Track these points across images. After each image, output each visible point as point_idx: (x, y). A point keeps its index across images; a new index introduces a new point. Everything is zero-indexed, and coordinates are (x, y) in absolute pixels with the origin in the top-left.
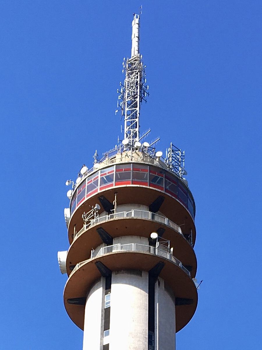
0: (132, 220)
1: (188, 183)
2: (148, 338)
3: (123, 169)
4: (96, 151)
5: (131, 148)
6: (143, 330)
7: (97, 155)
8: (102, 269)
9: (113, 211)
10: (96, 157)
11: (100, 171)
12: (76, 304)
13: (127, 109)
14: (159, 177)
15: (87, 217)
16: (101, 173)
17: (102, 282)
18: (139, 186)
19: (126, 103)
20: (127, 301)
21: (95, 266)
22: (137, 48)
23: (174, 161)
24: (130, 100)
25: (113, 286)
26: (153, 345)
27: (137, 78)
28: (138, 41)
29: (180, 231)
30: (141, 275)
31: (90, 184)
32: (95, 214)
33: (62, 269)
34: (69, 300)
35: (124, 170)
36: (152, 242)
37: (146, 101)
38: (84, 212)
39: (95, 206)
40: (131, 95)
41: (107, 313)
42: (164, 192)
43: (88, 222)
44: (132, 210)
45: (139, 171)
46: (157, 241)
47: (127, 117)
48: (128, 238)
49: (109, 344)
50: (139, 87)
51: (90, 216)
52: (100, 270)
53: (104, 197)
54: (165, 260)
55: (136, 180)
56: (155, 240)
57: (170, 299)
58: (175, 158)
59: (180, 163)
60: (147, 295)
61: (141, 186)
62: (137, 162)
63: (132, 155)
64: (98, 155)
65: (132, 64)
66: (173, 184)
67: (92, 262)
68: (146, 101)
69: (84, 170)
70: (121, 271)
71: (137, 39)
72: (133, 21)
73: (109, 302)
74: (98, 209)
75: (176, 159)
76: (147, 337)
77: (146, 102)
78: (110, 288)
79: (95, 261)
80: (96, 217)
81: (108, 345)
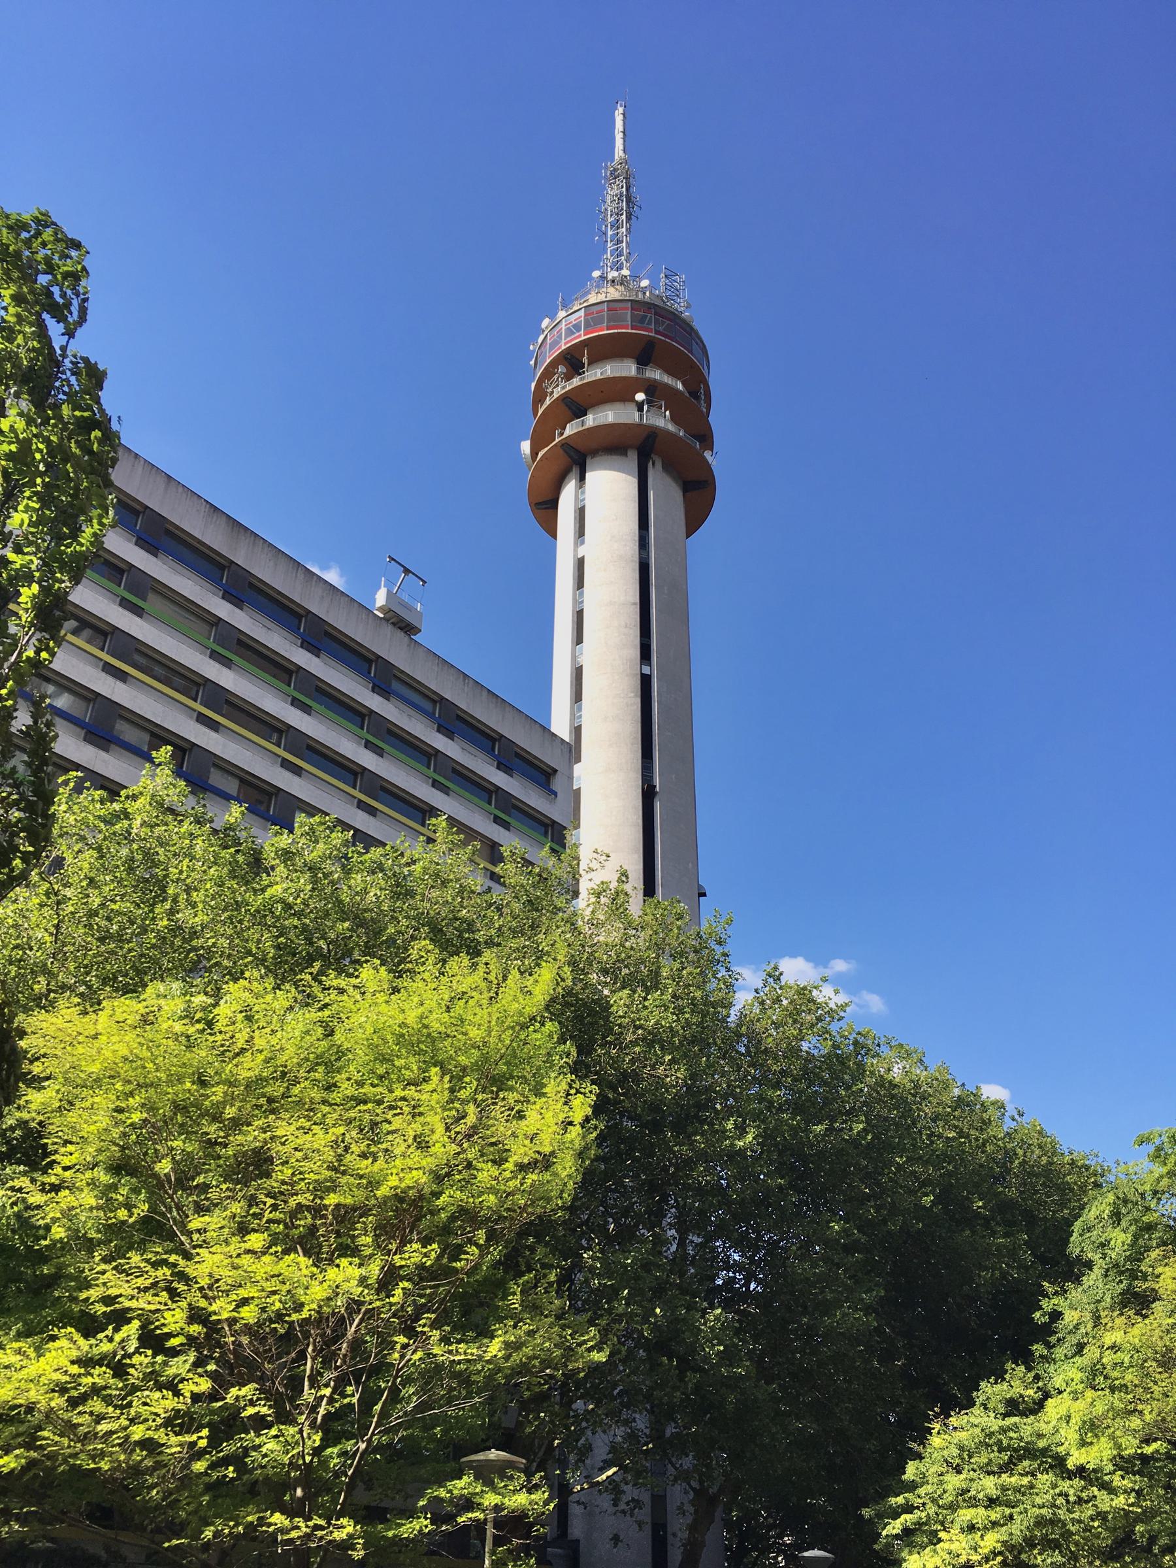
0: (608, 379)
12: (546, 507)
13: (610, 233)
17: (575, 472)
20: (606, 495)
21: (561, 452)
22: (621, 147)
25: (588, 475)
29: (680, 386)
30: (626, 455)
41: (581, 513)
48: (601, 407)
52: (570, 457)
56: (643, 402)
57: (674, 484)
69: (545, 322)
71: (621, 135)
76: (637, 538)
81: (583, 558)
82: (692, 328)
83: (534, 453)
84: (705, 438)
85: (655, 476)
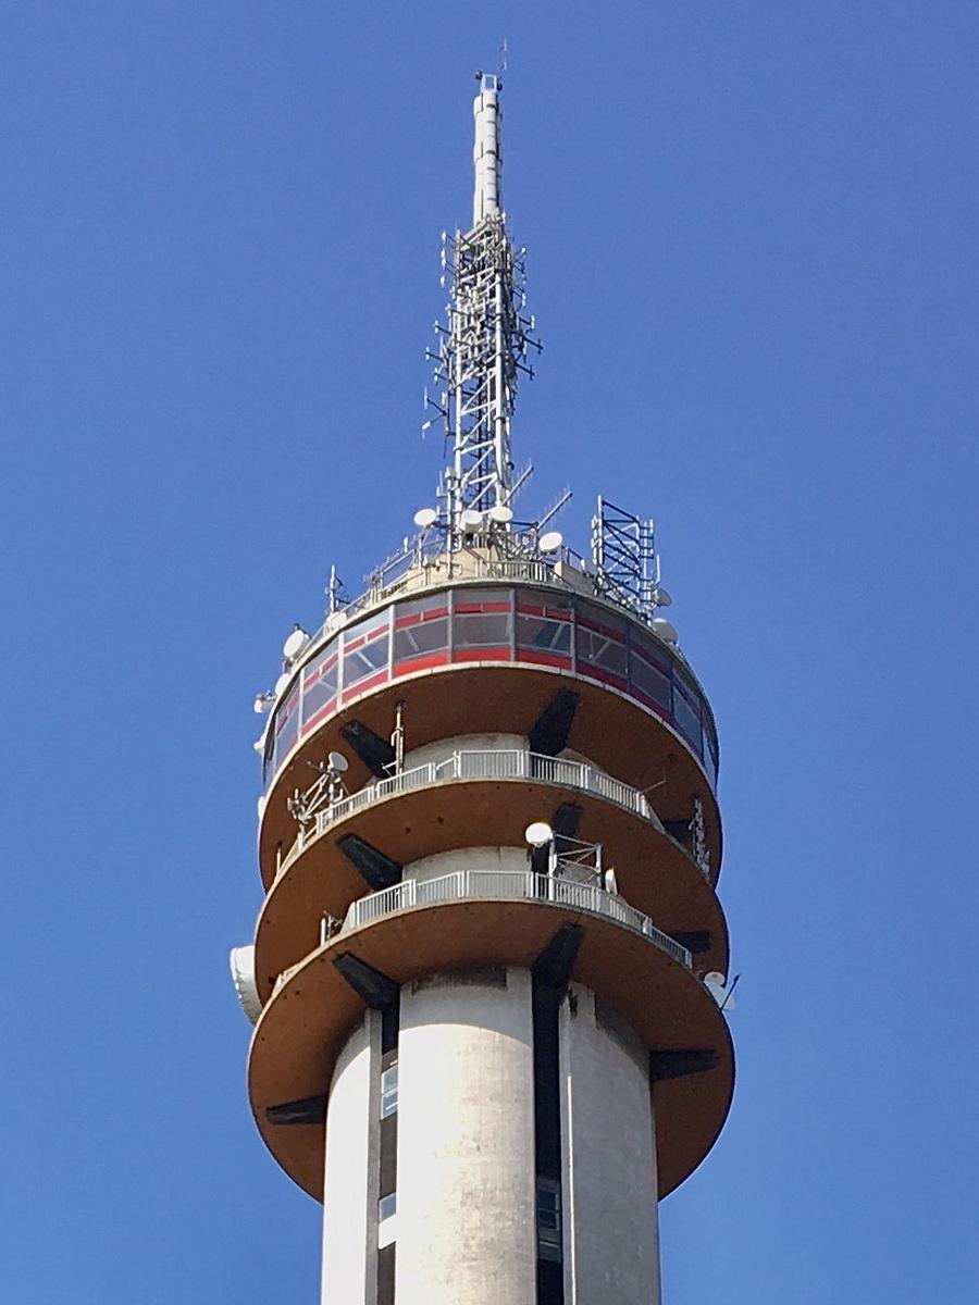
1: (675, 634)
2: (533, 1206)
3: (419, 615)
4: (333, 568)
5: (449, 536)
6: (516, 1176)
7: (338, 583)
8: (364, 981)
9: (394, 767)
10: (334, 591)
11: (341, 636)
12: (295, 1120)
13: (461, 412)
14: (604, 642)
15: (306, 807)
16: (346, 641)
17: (371, 1028)
18: (476, 664)
19: (459, 390)
20: (451, 1081)
22: (490, 192)
23: (616, 560)
24: (469, 377)
25: (405, 1036)
26: (558, 1228)
27: (493, 294)
28: (496, 165)
29: (642, 807)
31: (311, 687)
32: (331, 788)
33: (249, 1007)
34: (271, 1113)
35: (422, 618)
36: (538, 858)
37: (530, 372)
38: (297, 791)
39: (328, 763)
40: (473, 358)
42: (571, 673)
43: (312, 822)
44: (455, 753)
45: (479, 612)
46: (552, 850)
47: (462, 439)
48: (437, 861)
49: (394, 1244)
50: (498, 326)
51: (316, 801)
52: (355, 985)
53: (360, 725)
54: (582, 914)
55: (466, 645)
58: (620, 551)
59: (637, 563)
60: (529, 1049)
61: (485, 664)
62: (469, 581)
63: (452, 558)
64: (341, 584)
65: (474, 250)
66: (616, 643)
67: (322, 960)
68: (530, 372)
69: (295, 642)
70: (431, 980)
71: (489, 160)
72: (478, 100)
73: (394, 1098)
74: (341, 772)
75: (624, 554)
77: (532, 374)
78: (395, 1045)
79: (332, 955)
80: (336, 800)
81: (392, 1246)
82: (672, 657)
83: (265, 979)
84: (707, 940)
85: (578, 1037)
